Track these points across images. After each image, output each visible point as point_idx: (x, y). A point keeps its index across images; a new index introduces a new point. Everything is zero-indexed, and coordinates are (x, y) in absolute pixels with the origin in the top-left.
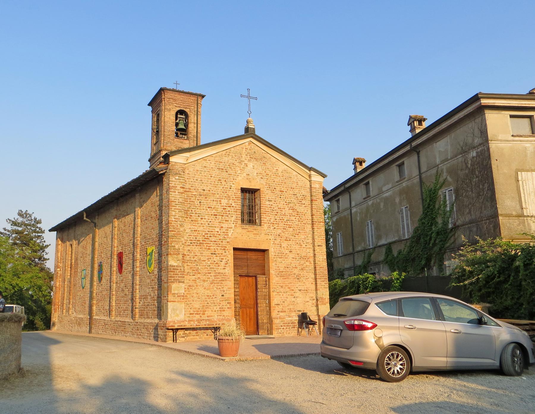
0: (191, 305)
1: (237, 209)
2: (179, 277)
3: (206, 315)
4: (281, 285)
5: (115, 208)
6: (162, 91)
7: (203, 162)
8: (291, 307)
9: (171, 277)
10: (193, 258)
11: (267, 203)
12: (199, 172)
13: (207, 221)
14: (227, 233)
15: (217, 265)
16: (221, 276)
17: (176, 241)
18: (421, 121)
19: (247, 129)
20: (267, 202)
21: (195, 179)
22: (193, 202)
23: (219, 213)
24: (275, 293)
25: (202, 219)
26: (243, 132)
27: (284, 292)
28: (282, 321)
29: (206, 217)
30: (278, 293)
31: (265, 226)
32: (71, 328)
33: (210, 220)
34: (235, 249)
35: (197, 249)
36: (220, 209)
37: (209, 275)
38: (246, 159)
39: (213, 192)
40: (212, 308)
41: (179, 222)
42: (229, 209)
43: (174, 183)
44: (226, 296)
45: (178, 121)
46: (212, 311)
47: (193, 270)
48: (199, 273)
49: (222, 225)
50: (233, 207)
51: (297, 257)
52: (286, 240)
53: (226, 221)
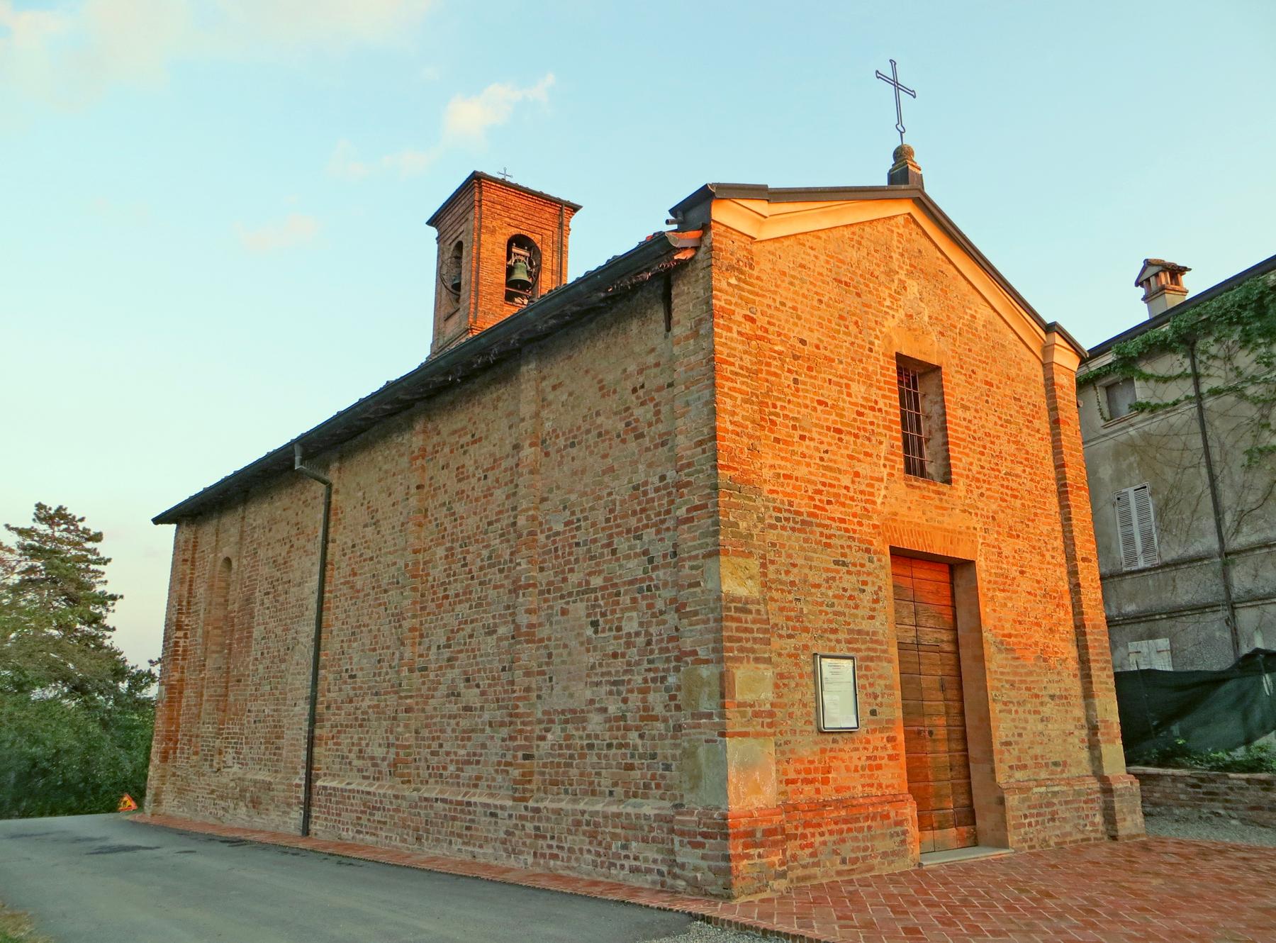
0: (786, 748)
1: (891, 421)
2: (755, 639)
3: (832, 784)
4: (1011, 678)
5: (418, 427)
6: (476, 180)
7: (797, 248)
8: (1038, 750)
9: (730, 639)
10: (787, 572)
11: (960, 413)
12: (787, 279)
13: (817, 449)
14: (872, 494)
15: (851, 603)
16: (864, 642)
17: (737, 506)
18: (1176, 272)
19: (903, 175)
20: (962, 405)
21: (778, 299)
22: (775, 374)
23: (848, 425)
24: (999, 707)
25: (802, 438)
26: (883, 182)
27: (1019, 703)
28: (1024, 800)
29: (815, 436)
30: (1005, 704)
31: (960, 485)
32: (221, 813)
33: (825, 447)
34: (900, 555)
35: (794, 541)
36: (850, 414)
37: (832, 636)
38: (901, 268)
39: (827, 353)
40: (846, 756)
41: (745, 440)
42: (870, 416)
43: (724, 297)
44: (884, 714)
45: (511, 263)
46: (848, 769)
47: (788, 618)
48: (806, 630)
49: (860, 468)
50: (880, 410)
51: (1038, 592)
52: (1011, 536)
53: (867, 454)
